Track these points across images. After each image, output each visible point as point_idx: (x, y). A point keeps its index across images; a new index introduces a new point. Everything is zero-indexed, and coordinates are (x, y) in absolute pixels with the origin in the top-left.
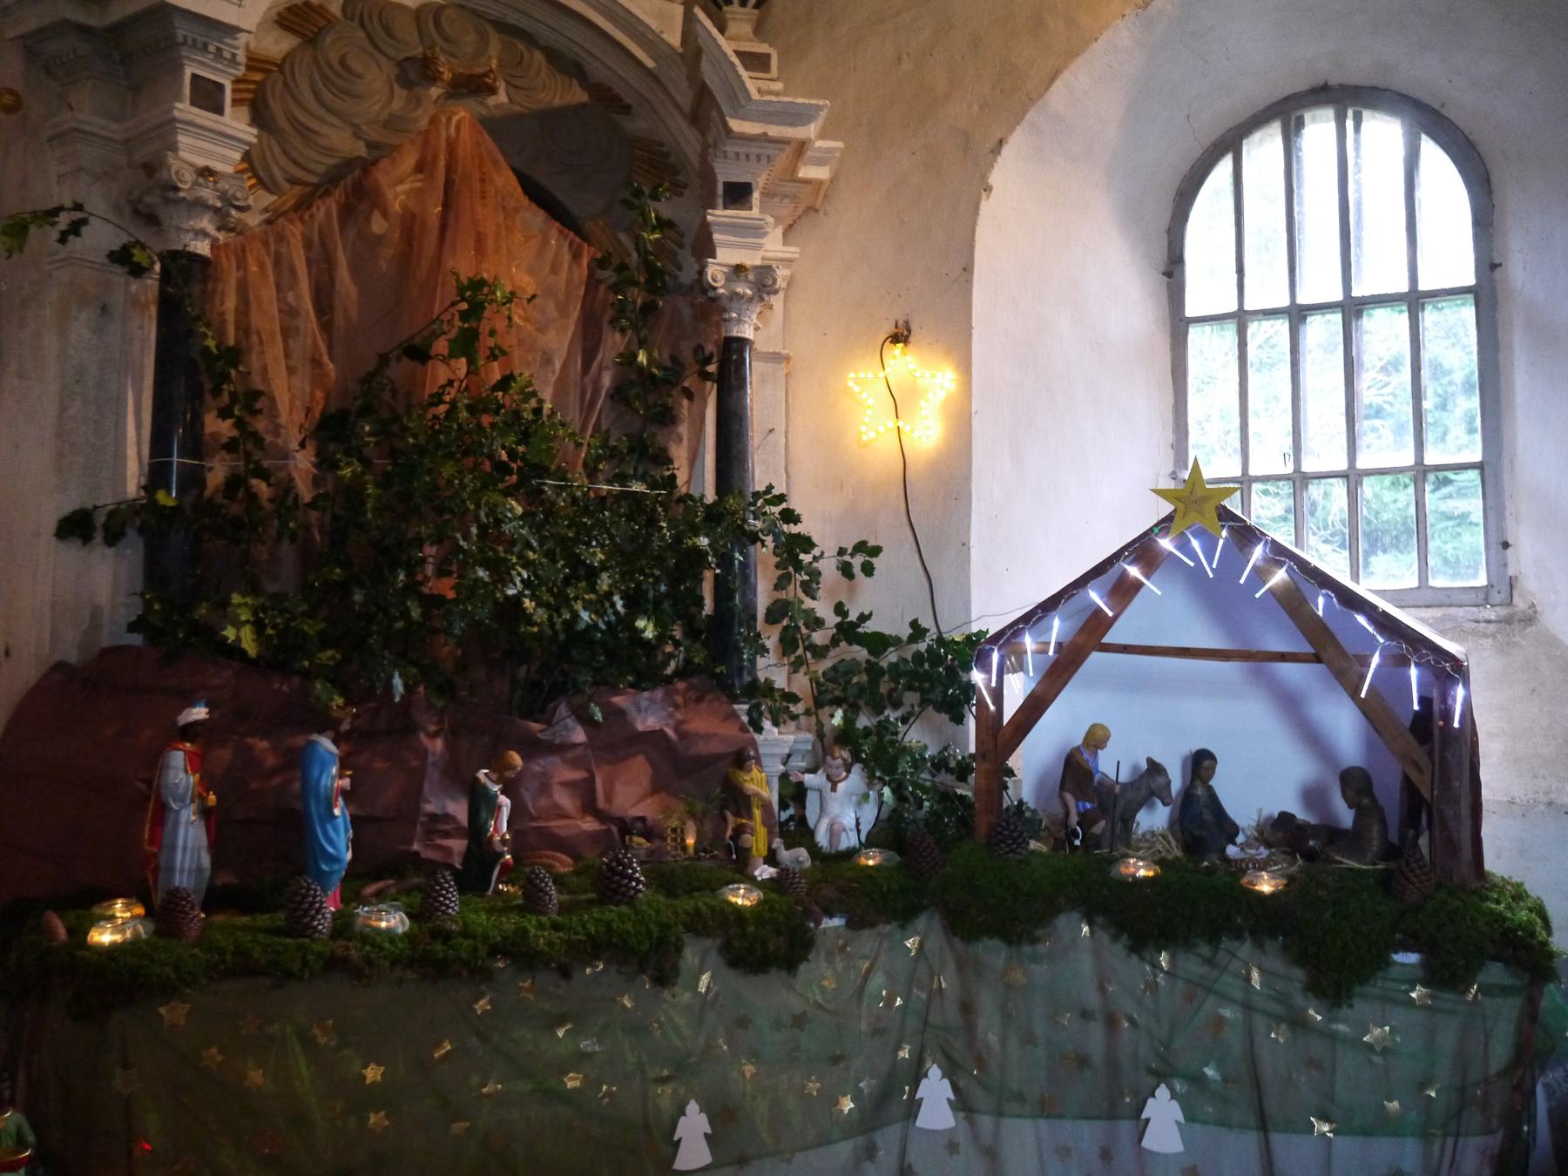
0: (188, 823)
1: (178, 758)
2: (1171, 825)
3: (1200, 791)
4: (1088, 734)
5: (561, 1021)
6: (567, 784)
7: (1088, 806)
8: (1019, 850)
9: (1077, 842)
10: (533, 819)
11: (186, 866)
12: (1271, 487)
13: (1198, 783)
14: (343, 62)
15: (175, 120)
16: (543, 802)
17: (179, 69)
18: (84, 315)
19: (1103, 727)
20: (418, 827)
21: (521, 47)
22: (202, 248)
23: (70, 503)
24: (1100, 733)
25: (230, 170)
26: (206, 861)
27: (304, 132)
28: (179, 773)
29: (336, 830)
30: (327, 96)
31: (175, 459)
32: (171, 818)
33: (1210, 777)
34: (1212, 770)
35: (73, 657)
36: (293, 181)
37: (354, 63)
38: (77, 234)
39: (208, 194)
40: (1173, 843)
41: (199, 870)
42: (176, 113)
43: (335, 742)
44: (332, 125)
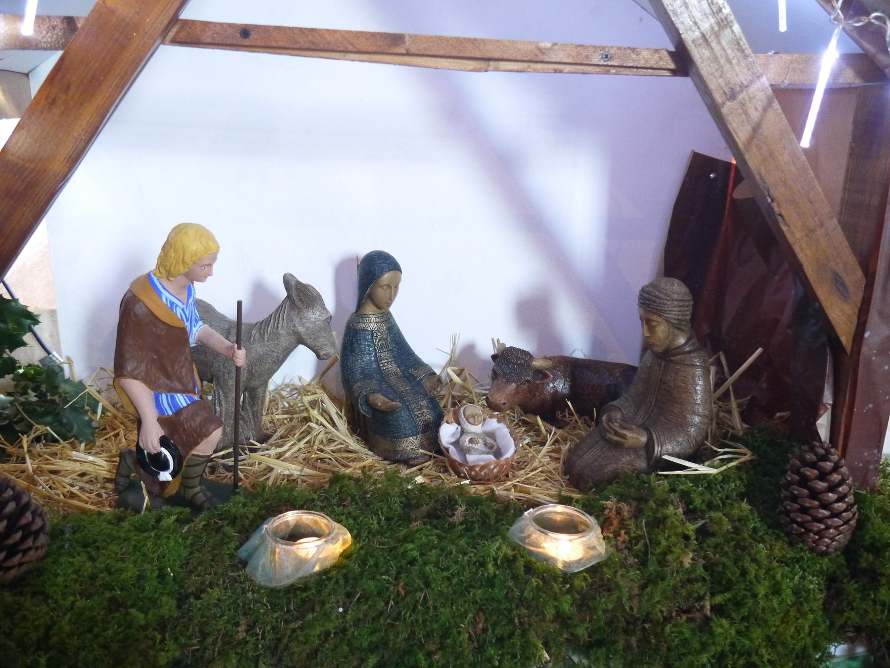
2: (321, 375)
3: (372, 323)
4: (167, 247)
7: (182, 400)
8: (29, 542)
9: (165, 476)
12: (326, 47)
13: (370, 309)
19: (202, 233)
24: (194, 246)
33: (389, 305)
34: (393, 287)
40: (333, 409)
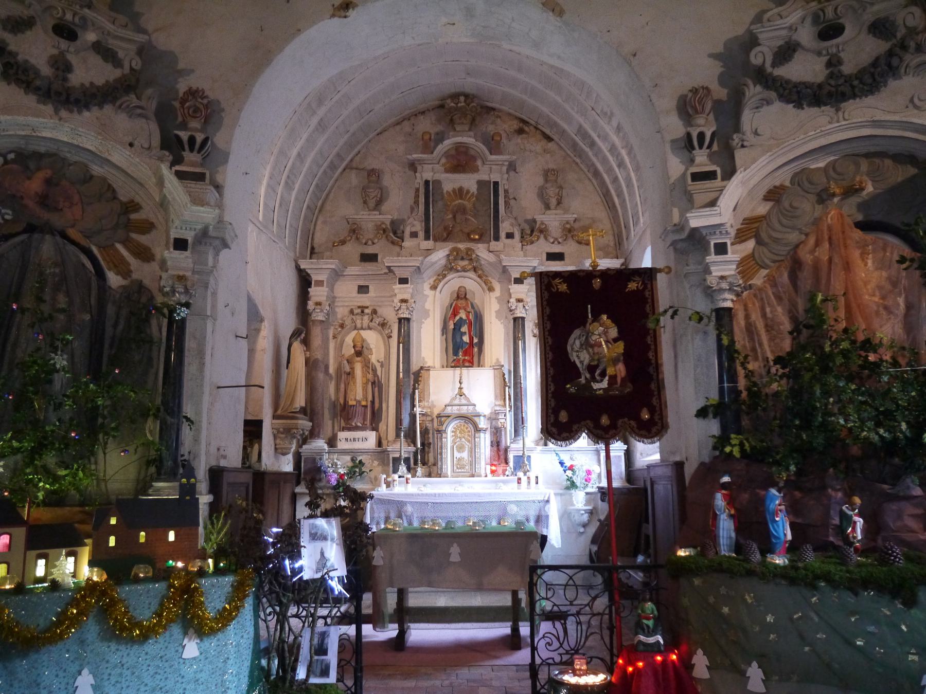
0: (724, 520)
1: (719, 496)
5: (853, 613)
6: (913, 516)
10: (893, 531)
11: (725, 536)
14: (791, 206)
15: (708, 263)
16: (899, 524)
17: (709, 243)
18: (698, 337)
20: (830, 530)
21: (877, 161)
22: (728, 304)
23: (701, 403)
25: (733, 273)
26: (733, 535)
27: (776, 240)
28: (719, 500)
29: (778, 526)
30: (784, 221)
31: (726, 385)
32: (718, 518)
35: (707, 460)
36: (774, 262)
37: (795, 204)
38: (676, 314)
39: (725, 285)
41: (730, 538)
42: (707, 261)
43: (779, 491)
44: (789, 233)
